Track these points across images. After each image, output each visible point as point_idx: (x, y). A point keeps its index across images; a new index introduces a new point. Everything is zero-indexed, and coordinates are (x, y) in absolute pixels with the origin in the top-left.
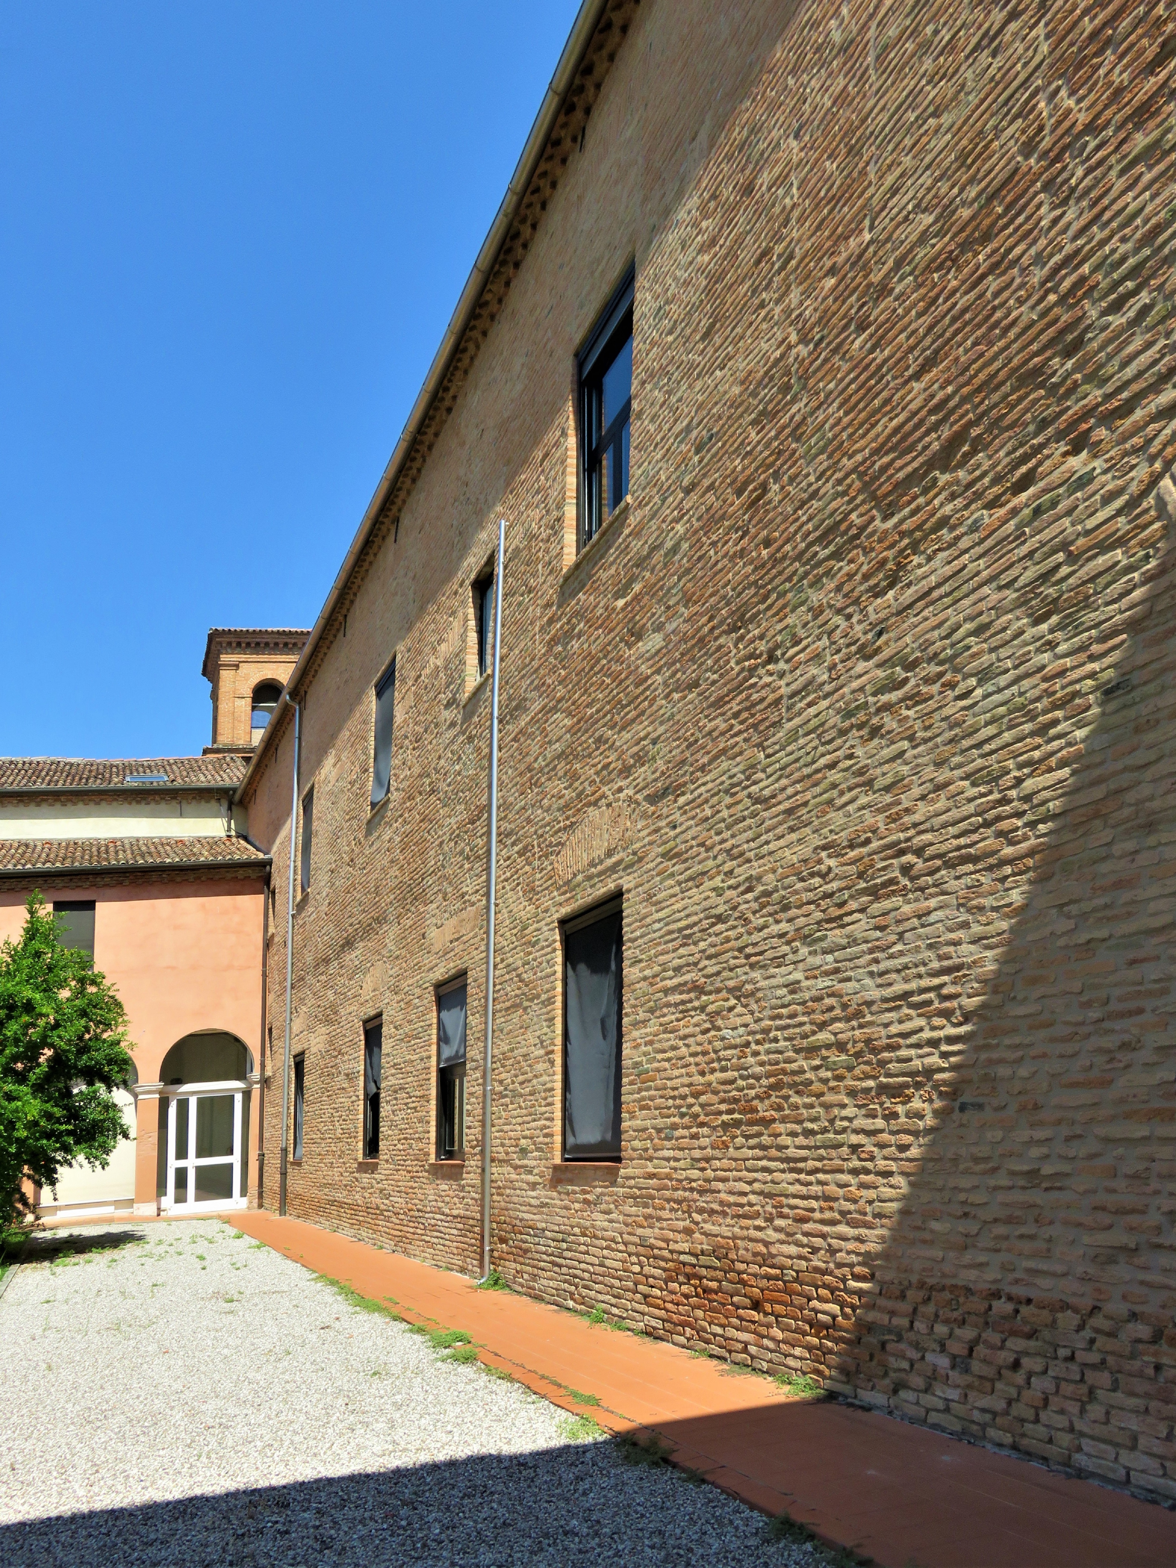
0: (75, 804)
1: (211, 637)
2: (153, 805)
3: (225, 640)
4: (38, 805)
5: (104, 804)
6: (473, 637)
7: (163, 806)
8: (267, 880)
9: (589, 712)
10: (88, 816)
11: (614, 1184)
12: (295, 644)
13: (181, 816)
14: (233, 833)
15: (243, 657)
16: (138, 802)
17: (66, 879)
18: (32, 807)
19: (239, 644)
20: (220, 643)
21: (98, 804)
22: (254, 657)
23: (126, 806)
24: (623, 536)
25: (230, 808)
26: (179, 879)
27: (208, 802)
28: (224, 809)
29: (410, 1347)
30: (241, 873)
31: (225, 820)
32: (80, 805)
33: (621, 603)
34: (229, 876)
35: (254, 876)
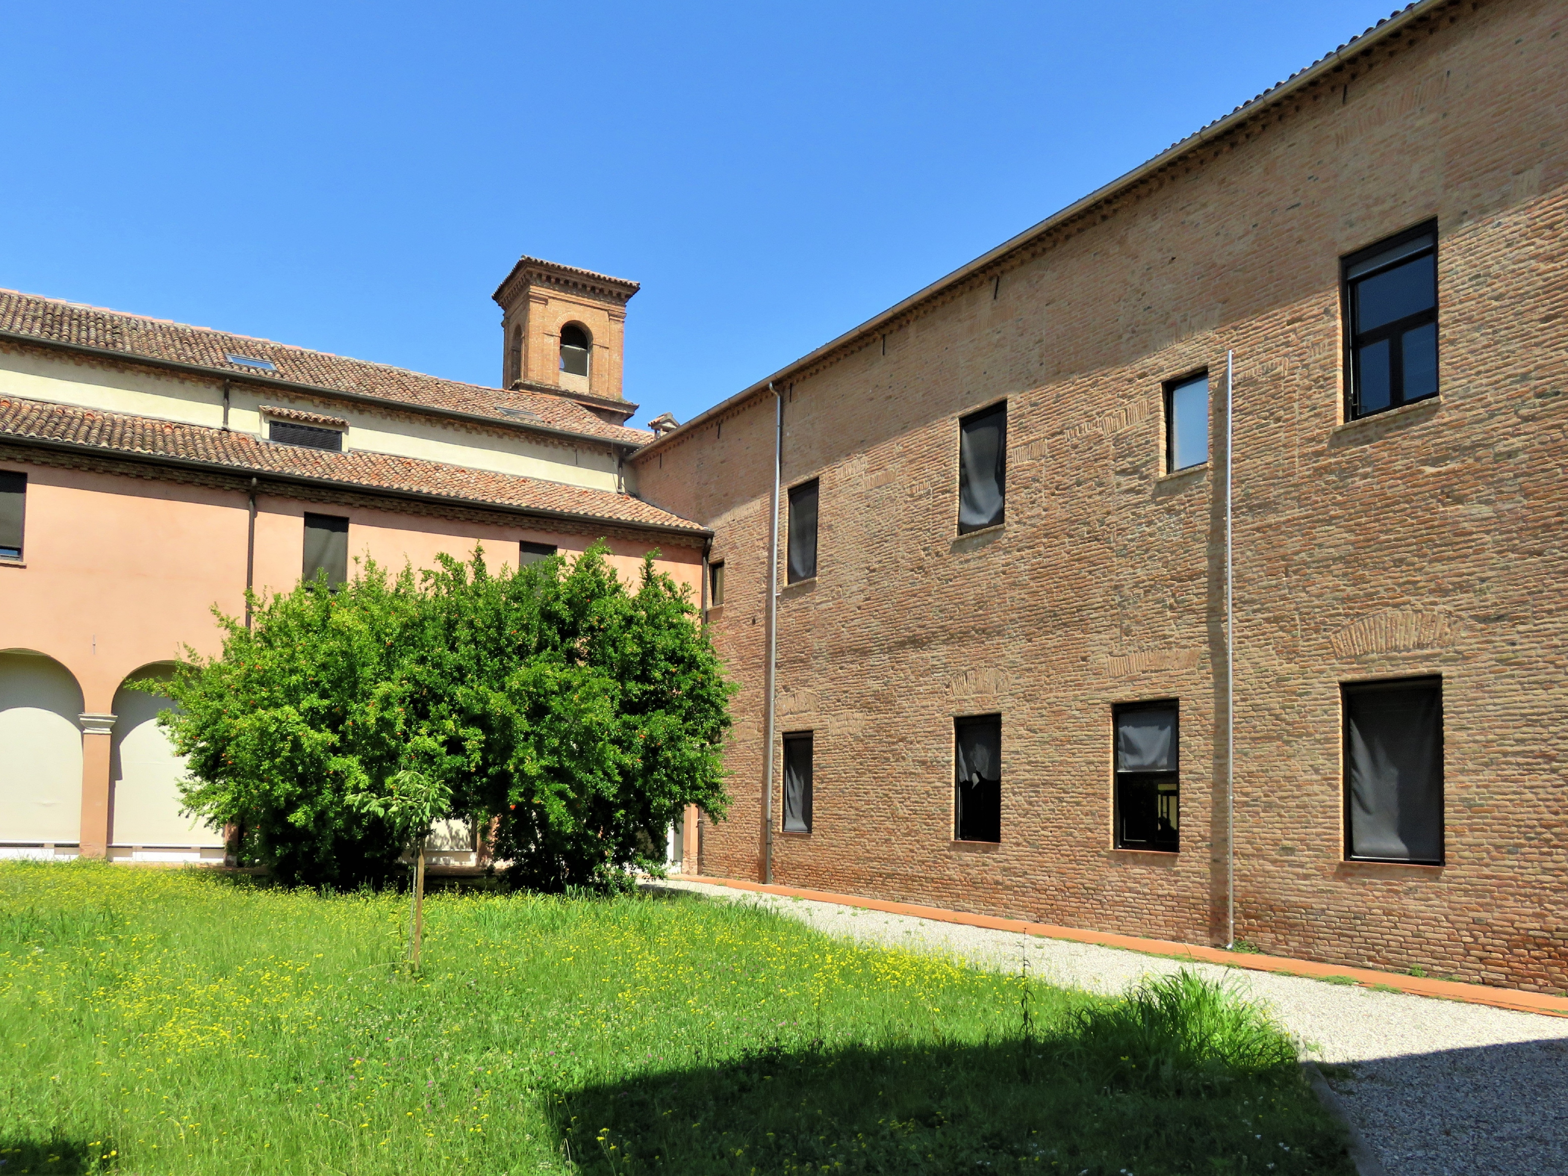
0: (479, 433)
1: (520, 265)
2: (550, 449)
3: (535, 271)
4: (445, 427)
5: (506, 438)
6: (1163, 426)
7: (560, 451)
8: (706, 551)
9: (1383, 537)
10: (492, 448)
11: (1437, 879)
12: (601, 290)
13: (577, 464)
14: (623, 490)
15: (552, 293)
16: (538, 443)
17: (534, 520)
18: (438, 429)
19: (549, 278)
20: (531, 273)
21: (500, 437)
22: (562, 295)
23: (526, 444)
24: (1429, 424)
25: (620, 466)
26: (630, 537)
27: (600, 454)
28: (616, 464)
29: (1312, 982)
30: (684, 541)
31: (616, 476)
32: (484, 436)
33: (1429, 470)
34: (674, 542)
35: (694, 546)
